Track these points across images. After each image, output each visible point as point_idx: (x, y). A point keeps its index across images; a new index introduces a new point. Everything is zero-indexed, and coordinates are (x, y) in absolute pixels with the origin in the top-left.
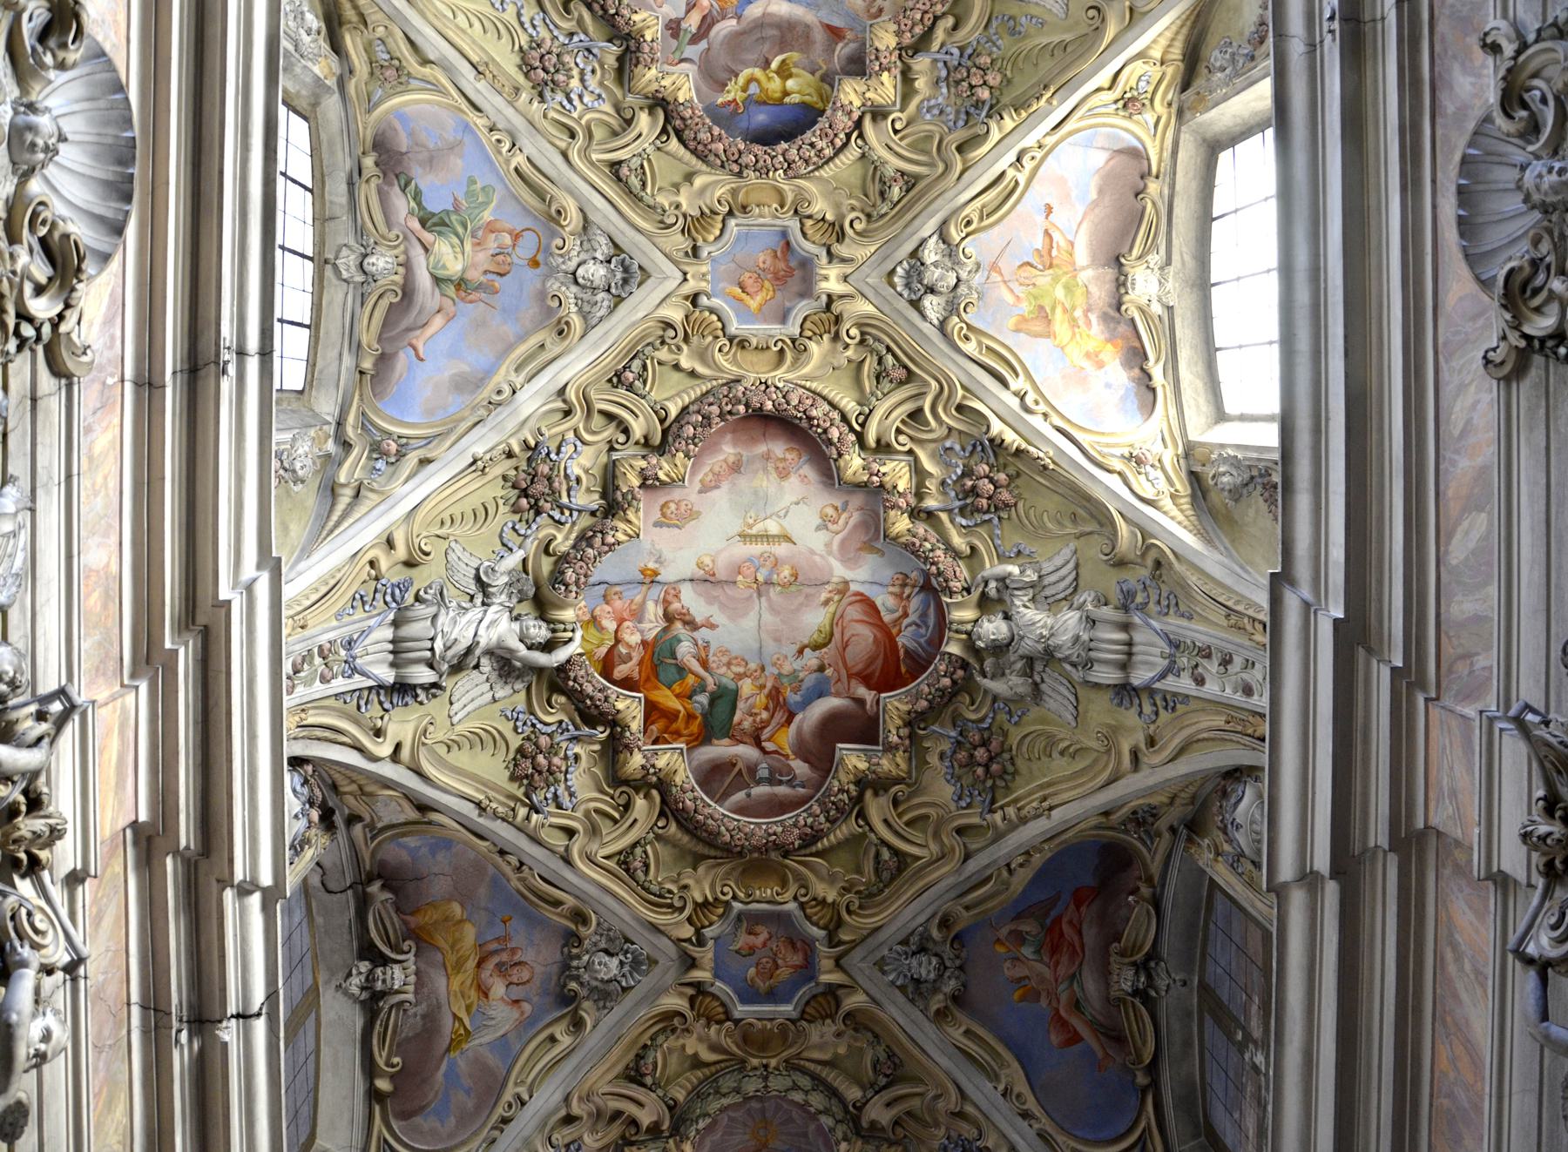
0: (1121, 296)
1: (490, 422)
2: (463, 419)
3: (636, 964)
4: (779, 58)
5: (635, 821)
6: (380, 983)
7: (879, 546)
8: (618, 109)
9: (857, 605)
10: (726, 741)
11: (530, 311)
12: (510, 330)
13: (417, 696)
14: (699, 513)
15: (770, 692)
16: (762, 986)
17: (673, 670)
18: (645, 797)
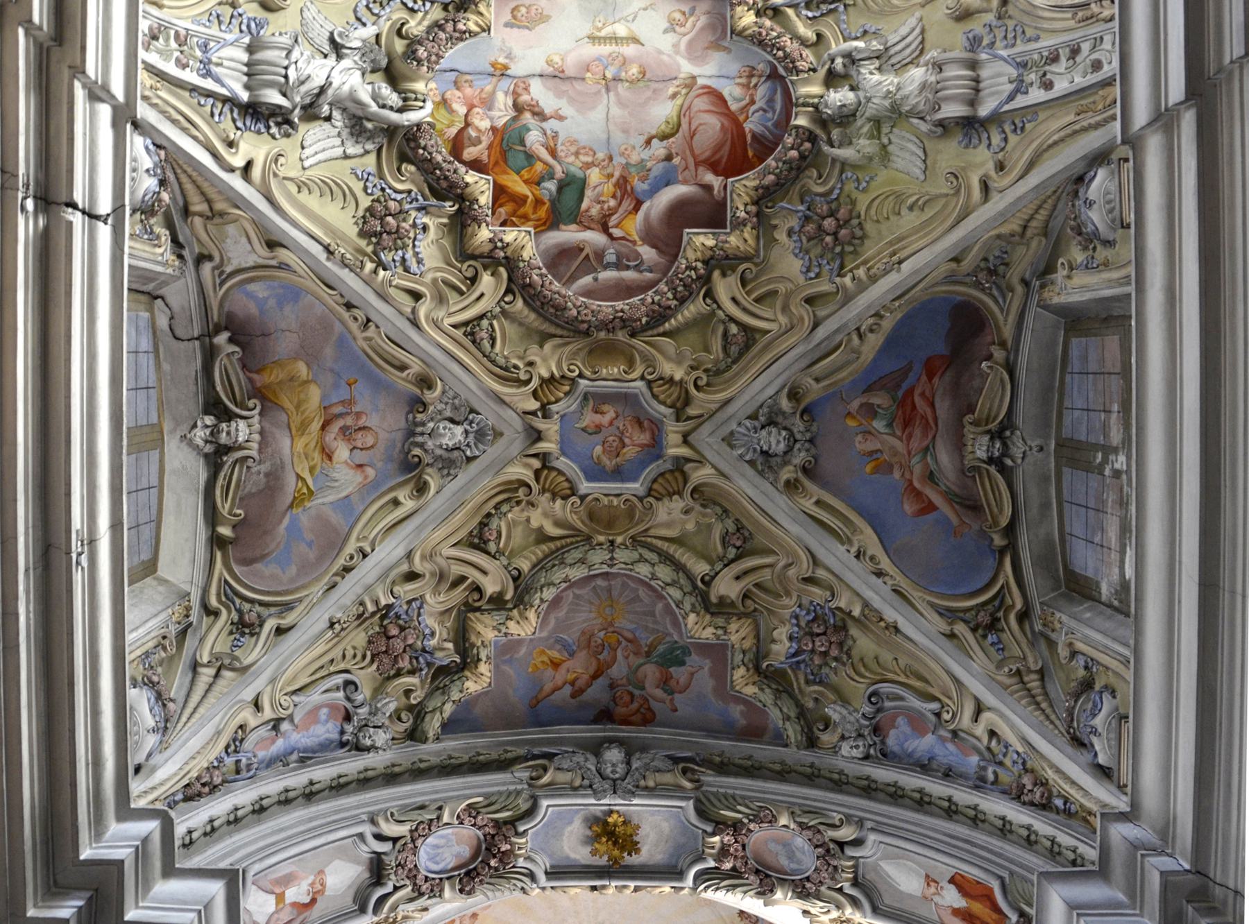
3: (480, 435)
5: (482, 295)
6: (224, 434)
7: (725, 44)
9: (705, 96)
10: (574, 227)
13: (268, 128)
14: (549, 17)
15: (618, 180)
16: (608, 463)
17: (522, 156)
18: (492, 275)
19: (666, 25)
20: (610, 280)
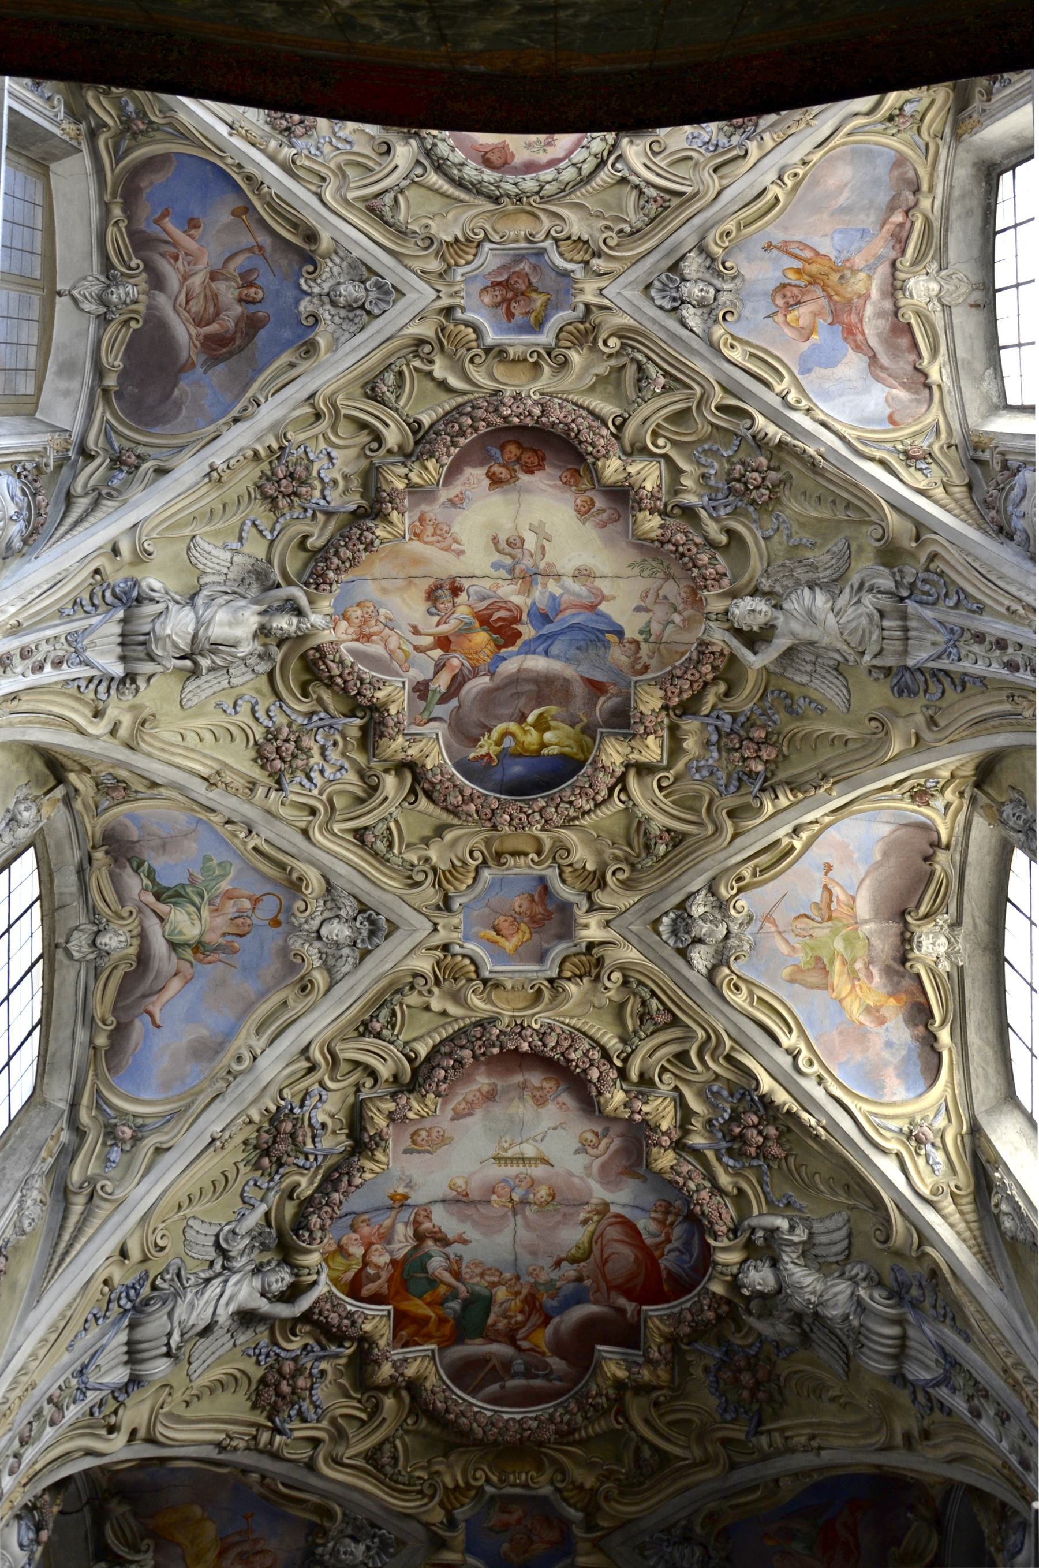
1: (230, 1095)
4: (536, 712)
5: (386, 798)
8: (361, 774)
10: (479, 1341)
11: (273, 967)
12: (250, 988)
14: (452, 1139)
20: (531, 671)
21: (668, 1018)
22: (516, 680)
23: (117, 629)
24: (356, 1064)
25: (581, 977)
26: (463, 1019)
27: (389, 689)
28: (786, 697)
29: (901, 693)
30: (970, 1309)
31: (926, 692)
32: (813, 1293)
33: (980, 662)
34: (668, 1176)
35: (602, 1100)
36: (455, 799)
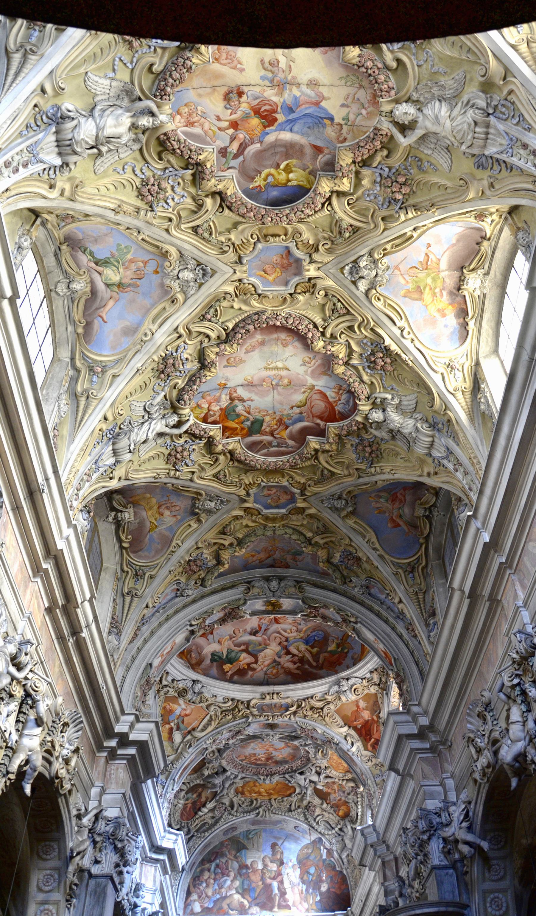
0: (460, 285)
1: (144, 351)
2: (130, 350)
4: (285, 163)
5: (207, 210)
8: (194, 199)
11: (157, 292)
12: (147, 302)
14: (245, 361)
19: (302, 363)
21: (346, 311)
22: (274, 145)
23: (53, 138)
24: (200, 333)
25: (305, 292)
26: (249, 311)
27: (206, 154)
28: (418, 161)
29: (478, 167)
30: (461, 435)
31: (491, 169)
32: (398, 423)
33: (522, 160)
34: (341, 376)
35: (313, 345)
36: (243, 210)
